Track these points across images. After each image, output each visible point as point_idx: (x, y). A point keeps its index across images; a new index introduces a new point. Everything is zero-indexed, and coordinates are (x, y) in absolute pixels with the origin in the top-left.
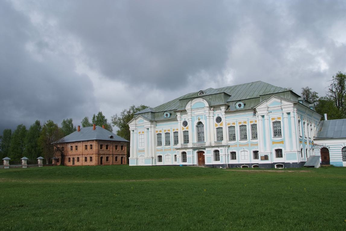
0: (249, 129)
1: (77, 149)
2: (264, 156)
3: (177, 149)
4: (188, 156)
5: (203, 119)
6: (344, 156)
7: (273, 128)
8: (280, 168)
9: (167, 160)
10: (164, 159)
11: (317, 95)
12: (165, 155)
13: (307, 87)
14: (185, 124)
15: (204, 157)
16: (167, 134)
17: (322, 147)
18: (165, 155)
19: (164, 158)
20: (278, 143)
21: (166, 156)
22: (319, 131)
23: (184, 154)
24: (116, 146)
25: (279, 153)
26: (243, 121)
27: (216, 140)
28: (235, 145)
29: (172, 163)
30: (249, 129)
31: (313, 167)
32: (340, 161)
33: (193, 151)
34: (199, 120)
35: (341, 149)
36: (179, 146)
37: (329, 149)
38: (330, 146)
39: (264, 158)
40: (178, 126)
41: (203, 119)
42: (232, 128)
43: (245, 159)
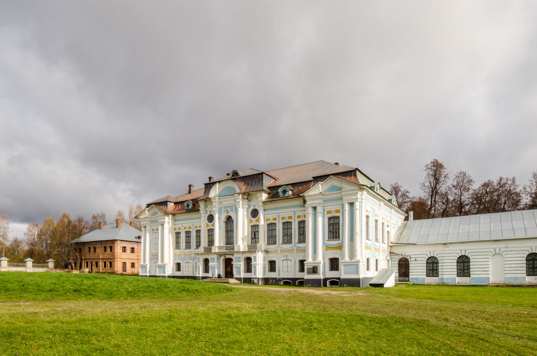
0: (295, 228)
1: (95, 252)
2: (312, 267)
3: (198, 254)
4: (211, 264)
5: (233, 212)
6: (428, 270)
7: (329, 226)
8: (8, 304)
9: (187, 269)
10: (183, 268)
11: (407, 194)
12: (184, 262)
13: (397, 183)
14: (211, 218)
15: (232, 266)
16: (188, 233)
17: (401, 257)
18: (184, 262)
19: (183, 266)
20: (334, 249)
21: (185, 263)
22: (399, 235)
23: (206, 261)
24: (105, 248)
25: (334, 264)
26: (287, 216)
27: (250, 244)
28: (276, 251)
29: (193, 274)
30: (295, 228)
31: (381, 285)
32: (423, 277)
33: (217, 258)
34: (228, 213)
35: (426, 260)
36: (201, 250)
37: (409, 260)
38: (412, 256)
39: (312, 271)
40: (202, 223)
41: (233, 212)
42: (271, 226)
43: (287, 272)
